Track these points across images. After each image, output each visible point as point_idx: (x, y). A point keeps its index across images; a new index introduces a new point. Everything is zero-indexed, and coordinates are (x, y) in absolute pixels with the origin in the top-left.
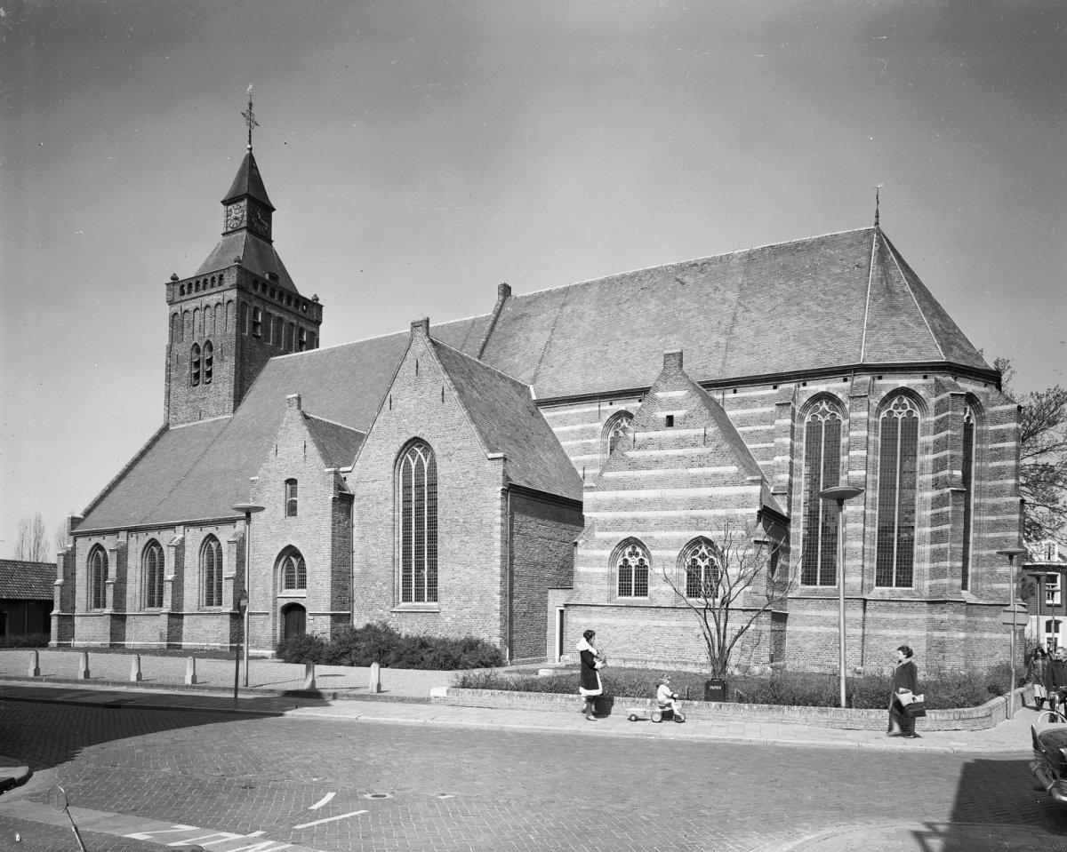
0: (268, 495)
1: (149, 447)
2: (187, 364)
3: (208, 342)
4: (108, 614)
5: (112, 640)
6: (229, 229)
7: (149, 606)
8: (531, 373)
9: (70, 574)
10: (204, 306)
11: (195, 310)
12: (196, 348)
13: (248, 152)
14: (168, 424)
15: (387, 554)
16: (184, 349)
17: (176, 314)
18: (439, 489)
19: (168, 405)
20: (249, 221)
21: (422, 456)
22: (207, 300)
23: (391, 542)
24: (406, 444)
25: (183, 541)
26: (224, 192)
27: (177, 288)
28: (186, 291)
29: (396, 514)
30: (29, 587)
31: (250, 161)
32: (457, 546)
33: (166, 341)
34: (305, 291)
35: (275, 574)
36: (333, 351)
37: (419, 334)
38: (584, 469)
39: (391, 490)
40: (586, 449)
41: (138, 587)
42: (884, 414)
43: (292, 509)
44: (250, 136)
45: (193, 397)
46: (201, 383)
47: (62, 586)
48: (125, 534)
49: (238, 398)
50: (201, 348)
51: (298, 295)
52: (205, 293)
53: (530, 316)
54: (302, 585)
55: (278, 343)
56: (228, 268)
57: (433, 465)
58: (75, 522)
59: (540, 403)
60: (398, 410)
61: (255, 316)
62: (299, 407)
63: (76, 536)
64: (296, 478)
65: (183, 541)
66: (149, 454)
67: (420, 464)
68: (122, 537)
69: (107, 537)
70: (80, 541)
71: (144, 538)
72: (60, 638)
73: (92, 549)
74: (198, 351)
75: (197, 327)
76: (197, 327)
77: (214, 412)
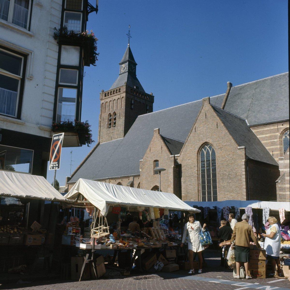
2: (107, 120)
3: (115, 112)
8: (246, 115)
10: (113, 100)
15: (196, 188)
16: (105, 116)
17: (103, 103)
18: (217, 162)
21: (209, 149)
22: (114, 98)
23: (197, 183)
24: (202, 145)
28: (107, 95)
29: (199, 172)
32: (226, 184)
34: (148, 91)
37: (206, 103)
38: (273, 152)
39: (196, 163)
40: (273, 144)
42: (284, 137)
44: (129, 41)
46: (112, 127)
48: (132, 177)
49: (126, 130)
50: (112, 115)
53: (242, 94)
57: (213, 152)
59: (251, 126)
60: (198, 132)
62: (159, 133)
64: (158, 159)
67: (208, 153)
69: (123, 179)
70: (70, 186)
77: (116, 137)
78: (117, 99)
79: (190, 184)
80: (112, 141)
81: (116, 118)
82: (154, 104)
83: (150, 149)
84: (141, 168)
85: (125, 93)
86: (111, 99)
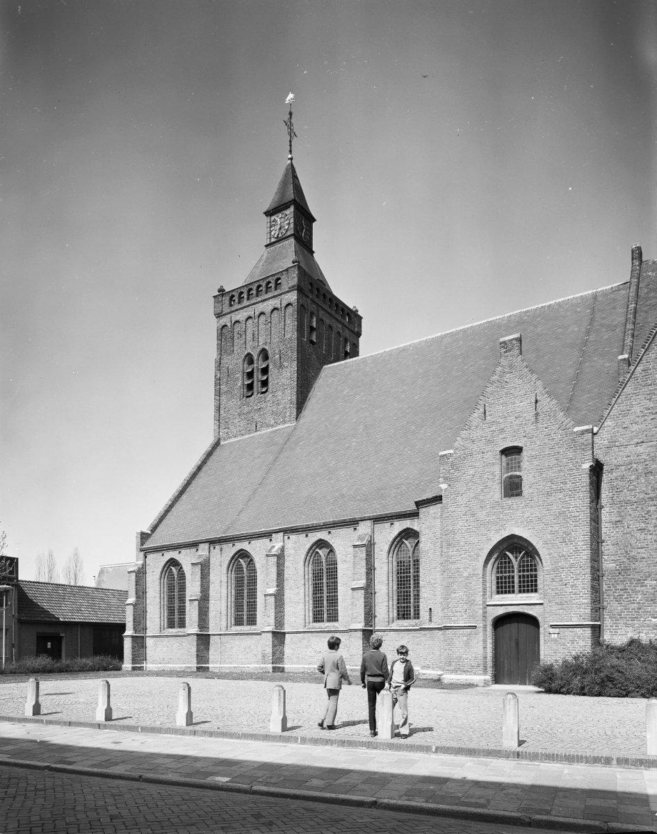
0: (472, 472)
1: (204, 462)
2: (239, 375)
4: (360, 630)
5: (198, 663)
6: (273, 240)
7: (236, 624)
9: (141, 593)
10: (257, 313)
11: (247, 320)
12: (249, 359)
13: (289, 161)
14: (219, 439)
16: (235, 362)
17: (226, 326)
19: (218, 419)
20: (295, 229)
22: (260, 307)
25: (283, 549)
26: (268, 202)
27: (226, 299)
30: (79, 610)
31: (292, 173)
33: (213, 354)
35: (484, 575)
36: (374, 359)
41: (224, 604)
43: (513, 487)
44: (291, 145)
45: (246, 409)
47: (135, 605)
48: (207, 546)
50: (255, 358)
51: (331, 293)
52: (259, 299)
54: (530, 585)
55: (328, 351)
56: (287, 270)
58: (144, 537)
61: (311, 322)
63: (146, 552)
64: (520, 445)
65: (283, 549)
66: (204, 469)
68: (203, 549)
70: (150, 556)
71: (230, 550)
72: (134, 661)
73: (165, 565)
74: (251, 362)
75: (249, 336)
76: (249, 336)
77: (272, 422)
78: (270, 311)
79: (642, 530)
80: (259, 433)
81: (268, 366)
82: (361, 339)
83: (482, 410)
84: (446, 479)
85: (296, 292)
86: (251, 314)
